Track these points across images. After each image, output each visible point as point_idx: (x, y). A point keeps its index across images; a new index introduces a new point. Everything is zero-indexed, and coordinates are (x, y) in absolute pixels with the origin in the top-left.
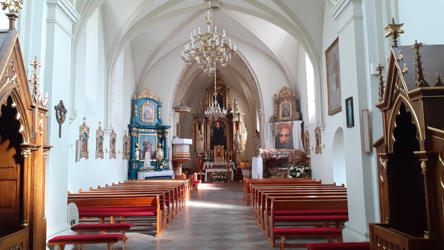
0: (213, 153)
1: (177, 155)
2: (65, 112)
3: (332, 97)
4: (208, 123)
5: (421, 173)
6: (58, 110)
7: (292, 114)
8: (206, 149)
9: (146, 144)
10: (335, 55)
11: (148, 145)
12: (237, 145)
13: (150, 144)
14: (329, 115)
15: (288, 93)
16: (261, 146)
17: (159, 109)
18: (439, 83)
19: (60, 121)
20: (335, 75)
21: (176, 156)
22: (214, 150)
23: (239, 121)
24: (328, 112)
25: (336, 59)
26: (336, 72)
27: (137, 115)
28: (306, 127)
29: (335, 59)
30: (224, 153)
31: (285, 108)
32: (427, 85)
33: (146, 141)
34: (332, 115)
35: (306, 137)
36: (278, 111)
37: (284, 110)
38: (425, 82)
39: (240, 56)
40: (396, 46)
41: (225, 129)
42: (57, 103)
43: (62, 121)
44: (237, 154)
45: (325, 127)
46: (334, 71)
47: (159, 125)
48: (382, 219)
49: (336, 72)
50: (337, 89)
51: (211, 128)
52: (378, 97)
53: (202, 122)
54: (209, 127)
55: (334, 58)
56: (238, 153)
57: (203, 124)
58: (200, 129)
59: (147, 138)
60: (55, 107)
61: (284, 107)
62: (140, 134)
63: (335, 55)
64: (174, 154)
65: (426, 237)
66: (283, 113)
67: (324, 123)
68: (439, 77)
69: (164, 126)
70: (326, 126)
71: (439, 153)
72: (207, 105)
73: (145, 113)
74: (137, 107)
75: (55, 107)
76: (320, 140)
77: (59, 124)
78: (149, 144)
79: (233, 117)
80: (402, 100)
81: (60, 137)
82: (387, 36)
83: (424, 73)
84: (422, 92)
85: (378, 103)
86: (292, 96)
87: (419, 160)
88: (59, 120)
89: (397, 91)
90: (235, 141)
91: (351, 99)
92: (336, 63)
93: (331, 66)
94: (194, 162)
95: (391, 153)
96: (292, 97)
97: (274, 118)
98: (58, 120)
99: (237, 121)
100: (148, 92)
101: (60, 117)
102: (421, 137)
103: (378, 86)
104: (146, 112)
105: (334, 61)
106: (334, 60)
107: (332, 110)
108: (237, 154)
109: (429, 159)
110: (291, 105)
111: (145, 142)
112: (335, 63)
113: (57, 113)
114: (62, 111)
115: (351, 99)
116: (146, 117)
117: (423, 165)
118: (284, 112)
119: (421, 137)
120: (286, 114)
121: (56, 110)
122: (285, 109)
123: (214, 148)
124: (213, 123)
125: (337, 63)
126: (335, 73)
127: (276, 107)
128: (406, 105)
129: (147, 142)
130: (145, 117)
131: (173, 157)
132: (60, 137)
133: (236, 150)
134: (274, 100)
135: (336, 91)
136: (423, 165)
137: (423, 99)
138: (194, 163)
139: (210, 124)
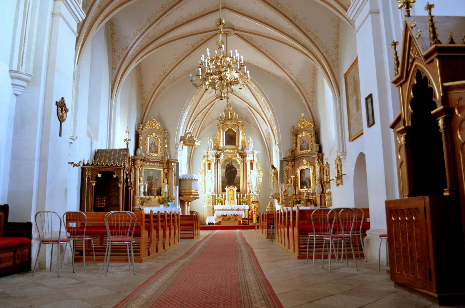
0: (225, 196)
2: (66, 111)
3: (352, 121)
4: (219, 163)
5: (439, 131)
6: (60, 107)
7: (311, 147)
8: (217, 191)
9: (150, 179)
10: (354, 77)
11: (153, 180)
12: (251, 187)
13: (155, 179)
18: (452, 42)
19: (61, 119)
20: (355, 98)
23: (253, 160)
26: (356, 94)
27: (141, 147)
28: (326, 159)
29: (355, 81)
30: (237, 195)
31: (304, 141)
32: (440, 43)
33: (151, 175)
34: (353, 141)
35: (326, 170)
36: (296, 144)
37: (302, 142)
38: (439, 41)
40: (409, 15)
42: (59, 100)
43: (63, 120)
45: (345, 155)
48: (401, 193)
49: (356, 94)
51: (222, 168)
52: (394, 72)
53: (212, 161)
54: (220, 167)
56: (253, 195)
59: (152, 172)
60: (56, 102)
62: (145, 168)
64: (181, 191)
65: (446, 194)
66: (301, 146)
67: (345, 151)
68: (452, 37)
71: (455, 107)
73: (151, 146)
74: (142, 138)
75: (56, 102)
77: (59, 122)
78: (154, 180)
79: (248, 156)
80: (418, 68)
81: (60, 135)
82: (400, 8)
83: (437, 32)
84: (437, 49)
85: (395, 78)
86: (311, 127)
88: (60, 117)
89: (413, 59)
90: (249, 182)
91: (371, 96)
92: (355, 85)
93: (351, 89)
95: (408, 126)
97: (292, 152)
98: (59, 117)
99: (251, 161)
101: (60, 114)
102: (438, 94)
103: (394, 57)
105: (353, 84)
106: (354, 81)
108: (252, 196)
109: (446, 114)
111: (149, 177)
113: (58, 109)
114: (63, 109)
115: (371, 96)
117: (441, 122)
118: (302, 145)
119: (438, 94)
120: (304, 147)
121: (58, 106)
122: (303, 142)
124: (224, 163)
125: (357, 85)
127: (293, 139)
128: (422, 70)
130: (150, 150)
131: (181, 194)
132: (60, 135)
134: (292, 132)
136: (441, 122)
137: (438, 57)
139: (221, 164)
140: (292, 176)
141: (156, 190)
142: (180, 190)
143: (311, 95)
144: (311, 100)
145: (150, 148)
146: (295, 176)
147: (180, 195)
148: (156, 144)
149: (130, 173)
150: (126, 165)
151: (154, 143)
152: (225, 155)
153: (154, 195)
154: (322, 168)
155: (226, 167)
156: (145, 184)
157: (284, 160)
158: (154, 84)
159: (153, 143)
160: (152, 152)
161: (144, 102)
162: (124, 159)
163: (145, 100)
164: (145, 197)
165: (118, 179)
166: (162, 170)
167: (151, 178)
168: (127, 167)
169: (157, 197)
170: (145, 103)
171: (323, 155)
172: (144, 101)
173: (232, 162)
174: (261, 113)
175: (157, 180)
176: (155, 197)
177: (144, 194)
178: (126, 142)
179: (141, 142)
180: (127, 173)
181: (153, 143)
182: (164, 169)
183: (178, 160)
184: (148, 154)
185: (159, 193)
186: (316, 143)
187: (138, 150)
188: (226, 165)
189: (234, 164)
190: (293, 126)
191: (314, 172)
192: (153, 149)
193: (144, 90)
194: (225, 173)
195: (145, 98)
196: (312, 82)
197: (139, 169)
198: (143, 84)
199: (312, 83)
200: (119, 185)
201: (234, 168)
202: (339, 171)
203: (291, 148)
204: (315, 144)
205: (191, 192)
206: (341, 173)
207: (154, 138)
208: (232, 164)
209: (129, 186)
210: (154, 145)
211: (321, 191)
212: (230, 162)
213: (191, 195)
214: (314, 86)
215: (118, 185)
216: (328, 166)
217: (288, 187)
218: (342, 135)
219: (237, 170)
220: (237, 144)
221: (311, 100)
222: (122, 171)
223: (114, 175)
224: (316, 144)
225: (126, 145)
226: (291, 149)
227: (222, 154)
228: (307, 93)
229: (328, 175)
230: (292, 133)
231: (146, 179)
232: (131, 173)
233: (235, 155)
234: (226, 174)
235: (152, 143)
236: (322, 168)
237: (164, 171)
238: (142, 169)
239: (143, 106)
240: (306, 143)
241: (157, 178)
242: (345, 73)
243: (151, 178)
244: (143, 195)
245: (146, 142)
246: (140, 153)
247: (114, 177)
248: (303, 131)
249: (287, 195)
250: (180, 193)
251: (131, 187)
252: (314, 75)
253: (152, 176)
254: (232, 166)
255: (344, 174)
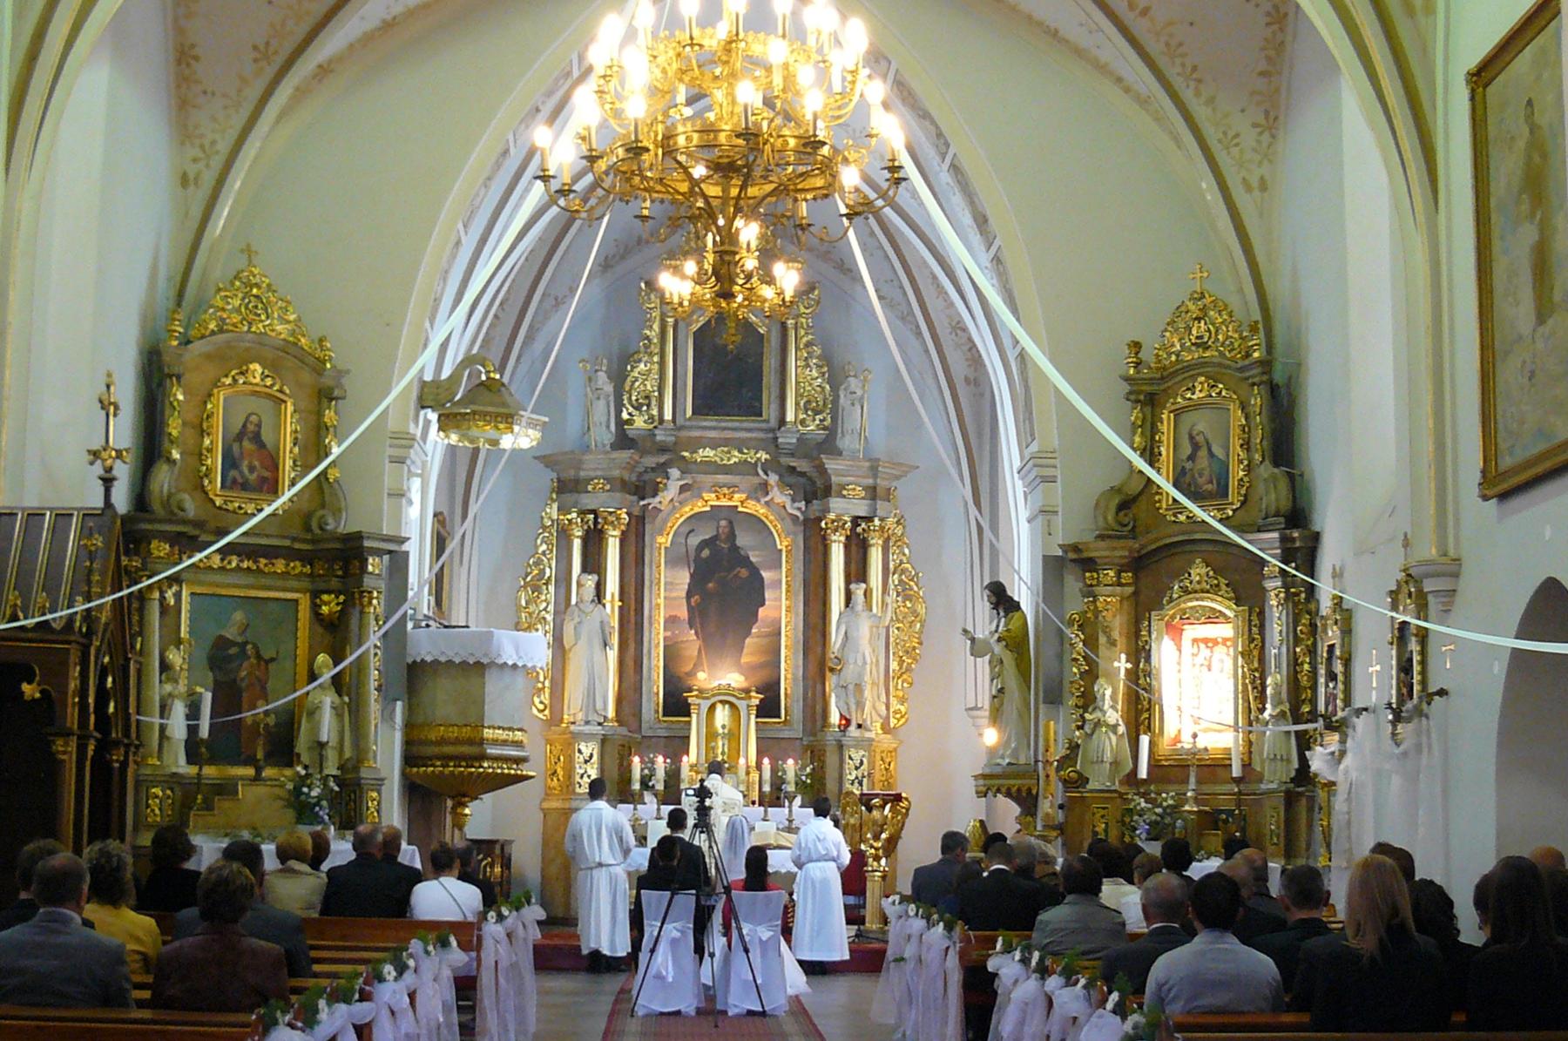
1: (442, 741)
9: (230, 659)
10: (1530, 103)
11: (245, 664)
13: (259, 656)
14: (1485, 498)
15: (1220, 337)
16: (864, 917)
17: (329, 416)
20: (1528, 235)
21: (436, 750)
22: (689, 715)
24: (1477, 477)
25: (1540, 127)
27: (176, 455)
29: (1533, 129)
31: (1200, 439)
33: (231, 633)
34: (1504, 496)
37: (1187, 450)
39: (938, 159)
41: (770, 568)
44: (853, 753)
46: (1525, 207)
47: (321, 528)
50: (1541, 330)
55: (1526, 121)
57: (617, 533)
58: (593, 563)
59: (238, 616)
61: (1191, 429)
63: (1530, 103)
66: (1183, 472)
67: (1452, 553)
69: (358, 537)
70: (1468, 569)
72: (647, 397)
73: (236, 447)
76: (1423, 663)
86: (1248, 355)
87: (547, 419)
92: (1537, 159)
94: (544, 800)
96: (1247, 362)
99: (856, 520)
100: (256, 297)
104: (240, 437)
105: (1521, 144)
106: (1526, 130)
107: (1507, 462)
110: (1238, 418)
111: (221, 643)
112: (1529, 158)
116: (241, 473)
118: (1188, 465)
120: (1200, 481)
122: (1196, 447)
123: (689, 705)
124: (686, 529)
125: (1544, 156)
126: (1532, 223)
129: (234, 644)
130: (233, 473)
131: (415, 749)
133: (847, 722)
134: (1127, 379)
135: (1534, 342)
138: (545, 805)
140: (1116, 664)
141: (267, 725)
142: (409, 726)
143: (1254, 150)
144: (1255, 182)
145: (230, 462)
146: (1137, 665)
147: (409, 760)
148: (266, 436)
149: (121, 661)
150: (98, 619)
151: (259, 425)
152: (689, 481)
153: (250, 761)
154: (1305, 619)
155: (692, 554)
156: (199, 689)
157: (1072, 555)
158: (262, 47)
159: (251, 428)
160: (245, 486)
161: (195, 160)
162: (89, 582)
163: (202, 147)
164: (193, 770)
165: (48, 705)
166: (305, 602)
167: (233, 651)
168: (107, 624)
169: (268, 772)
170: (201, 165)
171: (1316, 537)
172: (197, 152)
173: (731, 523)
174: (933, 226)
175: (272, 666)
176: (259, 770)
177: (191, 760)
178: (98, 469)
179: (174, 427)
180: (107, 659)
181: (251, 428)
182: (315, 594)
183: (404, 540)
184: (218, 502)
185: (282, 744)
186: (1276, 464)
187: (155, 470)
188: (694, 541)
189: (743, 540)
190: (1136, 346)
191: (1258, 642)
192: (252, 469)
193: (198, 82)
194: (689, 595)
195: (202, 136)
196: (1263, 66)
197: (163, 598)
198: (193, 46)
199: (1263, 74)
200: (59, 746)
201: (746, 562)
202: (1410, 660)
203: (1115, 483)
204: (1266, 470)
205: (482, 742)
206: (1424, 683)
207: (255, 393)
208: (732, 536)
209: (117, 743)
210: (257, 438)
211: (1296, 765)
212: (723, 523)
213: (483, 757)
214: (1278, 90)
215: (49, 744)
216: (1345, 616)
217: (1088, 728)
218: (1440, 446)
219: (767, 575)
220: (770, 411)
221: (1255, 182)
222: (74, 657)
223: (26, 687)
224: (1276, 470)
225: (99, 489)
226: (1114, 490)
227: (674, 473)
228: (1231, 134)
229: (1340, 678)
230: (1127, 388)
231: (202, 656)
232: (128, 660)
233: (756, 480)
234: (695, 599)
235: (244, 426)
236: (1305, 619)
237: (315, 608)
238: (178, 596)
239: (192, 188)
240: (1211, 454)
241: (267, 655)
242: (1473, 59)
243: (233, 651)
244: (182, 758)
245: (205, 425)
246: (170, 496)
247: (27, 696)
248: (1194, 378)
249: (1082, 780)
250: (408, 743)
251: (127, 746)
252: (1276, 27)
253: (239, 639)
254: (735, 548)
255: (1442, 693)
